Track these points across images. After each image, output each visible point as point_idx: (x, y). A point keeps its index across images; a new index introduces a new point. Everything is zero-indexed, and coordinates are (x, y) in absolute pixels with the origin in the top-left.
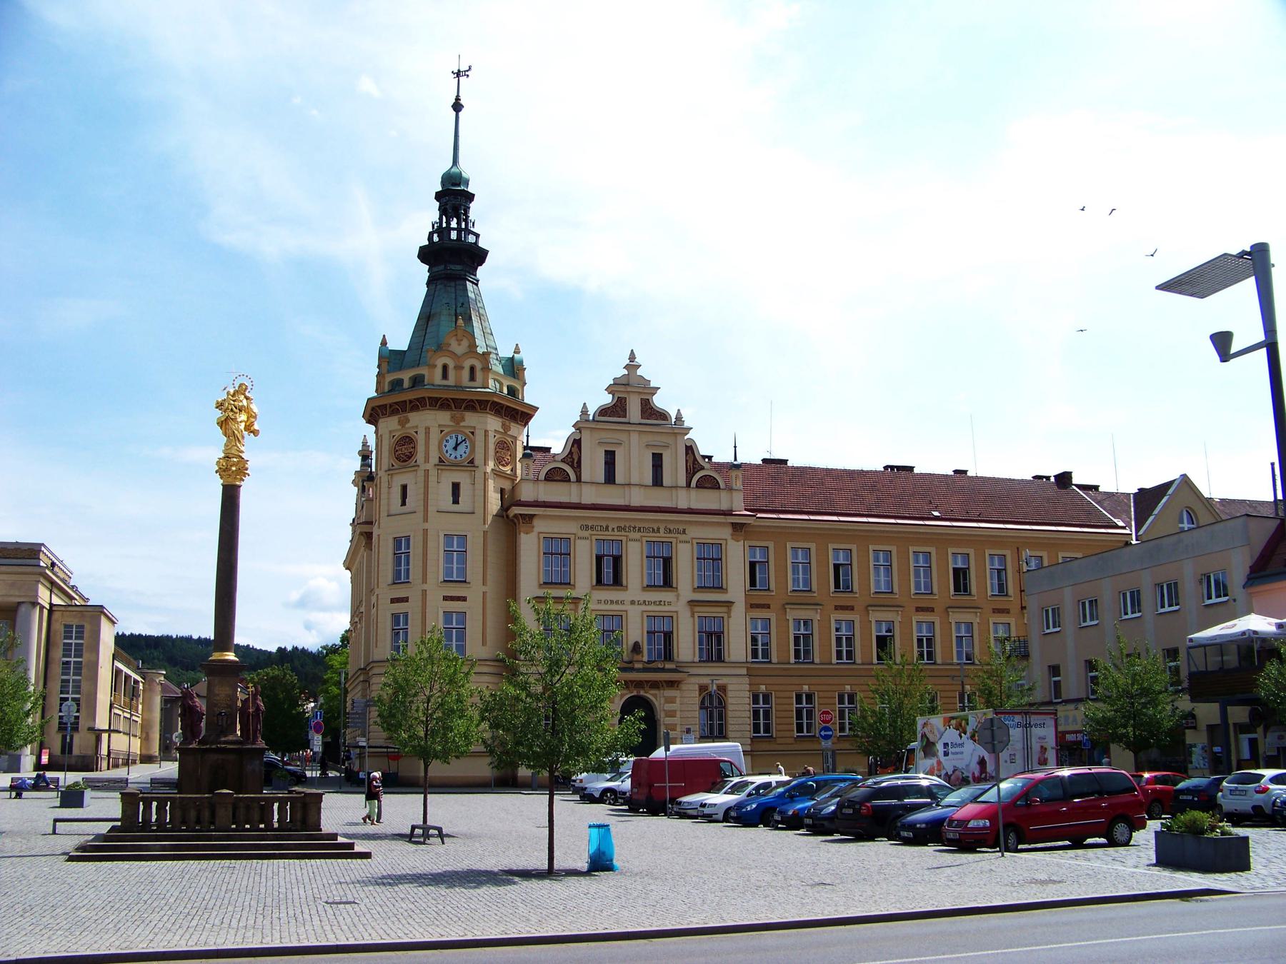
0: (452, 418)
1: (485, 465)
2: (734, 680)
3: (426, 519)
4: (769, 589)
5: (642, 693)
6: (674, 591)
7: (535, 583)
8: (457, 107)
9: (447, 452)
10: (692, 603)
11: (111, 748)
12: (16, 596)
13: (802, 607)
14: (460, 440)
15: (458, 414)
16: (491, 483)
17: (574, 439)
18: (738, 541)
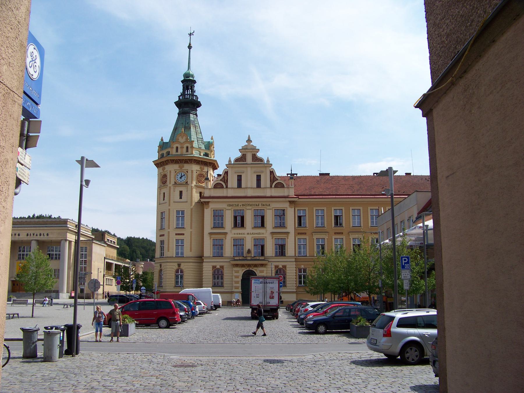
0: (179, 167)
1: (192, 183)
2: (289, 263)
3: (169, 205)
4: (306, 227)
5: (251, 269)
6: (265, 229)
7: (210, 228)
8: (190, 47)
9: (178, 179)
10: (272, 233)
11: (104, 291)
12: (60, 237)
13: (318, 233)
14: (182, 175)
15: (181, 165)
16: (194, 190)
17: (225, 172)
18: (292, 208)
